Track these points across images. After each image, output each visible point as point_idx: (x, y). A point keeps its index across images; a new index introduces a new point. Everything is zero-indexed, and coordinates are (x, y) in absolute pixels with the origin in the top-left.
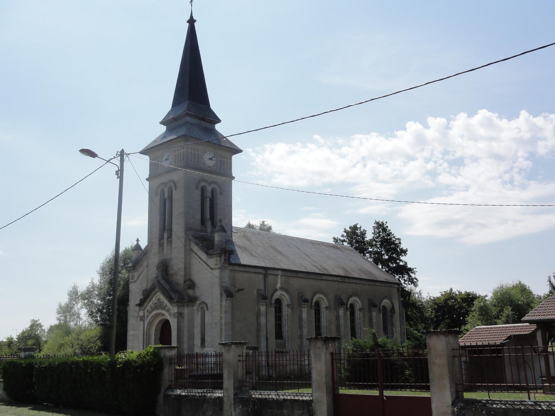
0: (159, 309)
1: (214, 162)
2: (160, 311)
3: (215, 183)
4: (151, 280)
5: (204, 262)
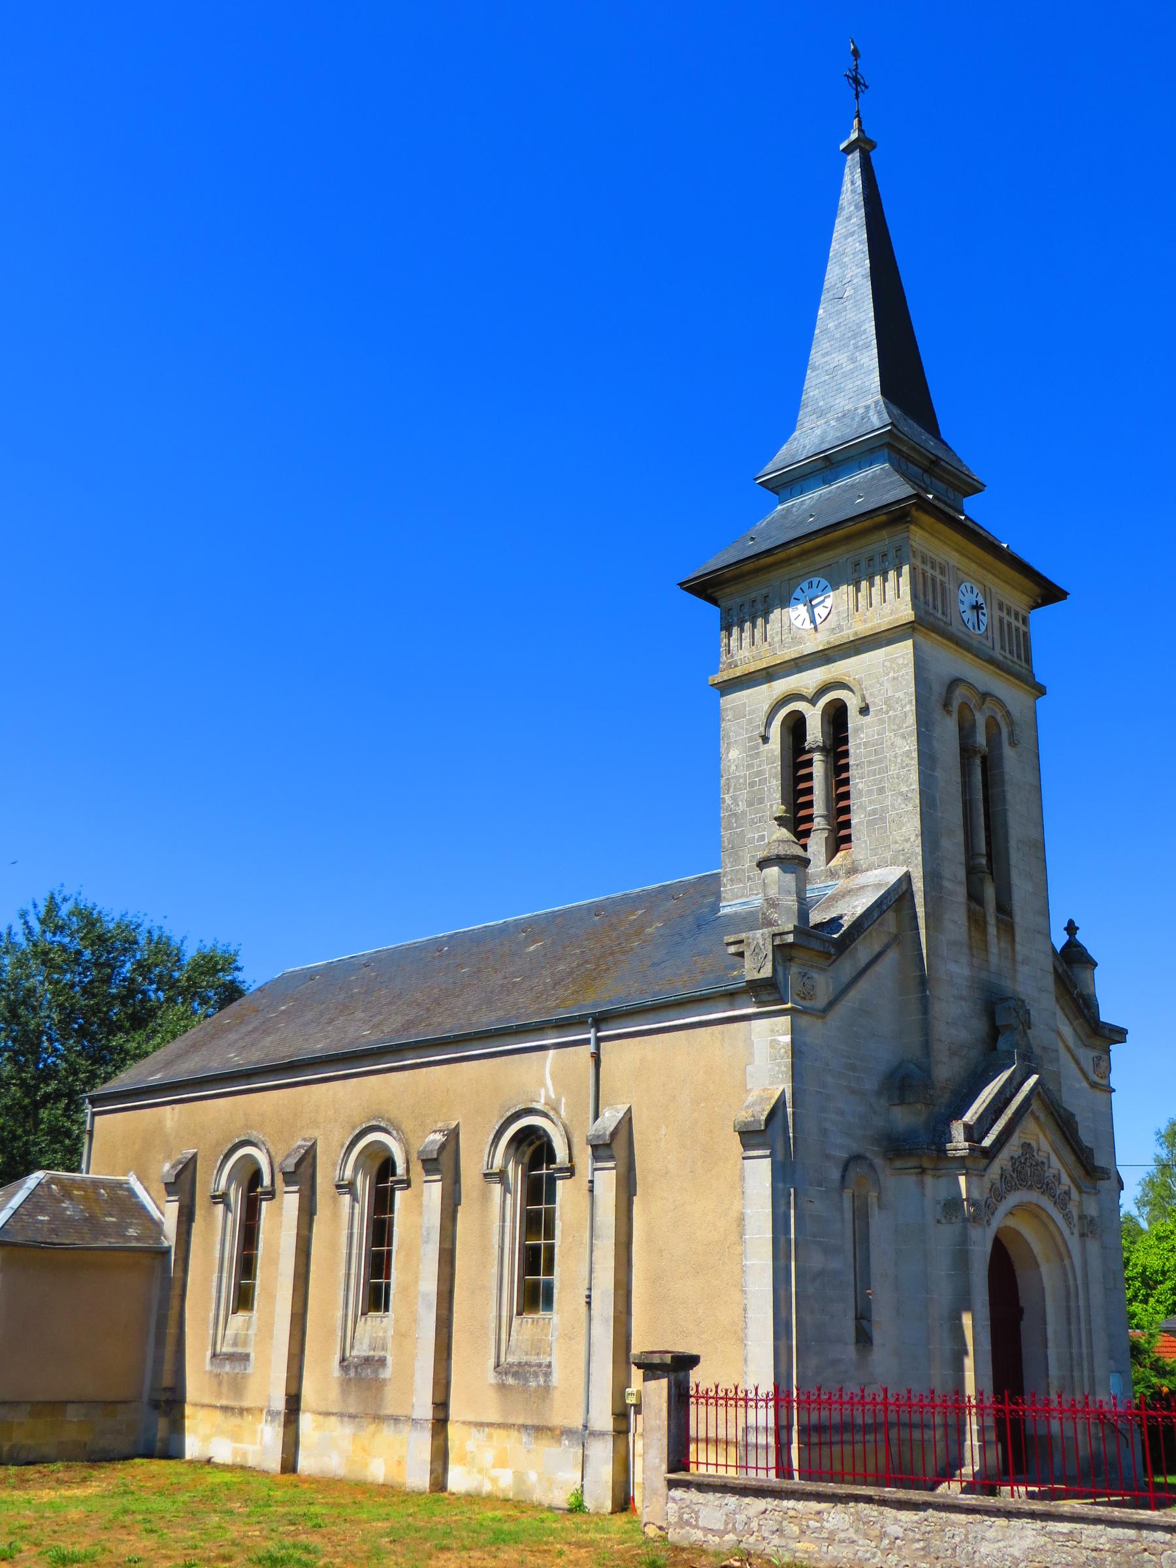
0: (1030, 1187)
2: (1033, 1196)
3: (999, 701)
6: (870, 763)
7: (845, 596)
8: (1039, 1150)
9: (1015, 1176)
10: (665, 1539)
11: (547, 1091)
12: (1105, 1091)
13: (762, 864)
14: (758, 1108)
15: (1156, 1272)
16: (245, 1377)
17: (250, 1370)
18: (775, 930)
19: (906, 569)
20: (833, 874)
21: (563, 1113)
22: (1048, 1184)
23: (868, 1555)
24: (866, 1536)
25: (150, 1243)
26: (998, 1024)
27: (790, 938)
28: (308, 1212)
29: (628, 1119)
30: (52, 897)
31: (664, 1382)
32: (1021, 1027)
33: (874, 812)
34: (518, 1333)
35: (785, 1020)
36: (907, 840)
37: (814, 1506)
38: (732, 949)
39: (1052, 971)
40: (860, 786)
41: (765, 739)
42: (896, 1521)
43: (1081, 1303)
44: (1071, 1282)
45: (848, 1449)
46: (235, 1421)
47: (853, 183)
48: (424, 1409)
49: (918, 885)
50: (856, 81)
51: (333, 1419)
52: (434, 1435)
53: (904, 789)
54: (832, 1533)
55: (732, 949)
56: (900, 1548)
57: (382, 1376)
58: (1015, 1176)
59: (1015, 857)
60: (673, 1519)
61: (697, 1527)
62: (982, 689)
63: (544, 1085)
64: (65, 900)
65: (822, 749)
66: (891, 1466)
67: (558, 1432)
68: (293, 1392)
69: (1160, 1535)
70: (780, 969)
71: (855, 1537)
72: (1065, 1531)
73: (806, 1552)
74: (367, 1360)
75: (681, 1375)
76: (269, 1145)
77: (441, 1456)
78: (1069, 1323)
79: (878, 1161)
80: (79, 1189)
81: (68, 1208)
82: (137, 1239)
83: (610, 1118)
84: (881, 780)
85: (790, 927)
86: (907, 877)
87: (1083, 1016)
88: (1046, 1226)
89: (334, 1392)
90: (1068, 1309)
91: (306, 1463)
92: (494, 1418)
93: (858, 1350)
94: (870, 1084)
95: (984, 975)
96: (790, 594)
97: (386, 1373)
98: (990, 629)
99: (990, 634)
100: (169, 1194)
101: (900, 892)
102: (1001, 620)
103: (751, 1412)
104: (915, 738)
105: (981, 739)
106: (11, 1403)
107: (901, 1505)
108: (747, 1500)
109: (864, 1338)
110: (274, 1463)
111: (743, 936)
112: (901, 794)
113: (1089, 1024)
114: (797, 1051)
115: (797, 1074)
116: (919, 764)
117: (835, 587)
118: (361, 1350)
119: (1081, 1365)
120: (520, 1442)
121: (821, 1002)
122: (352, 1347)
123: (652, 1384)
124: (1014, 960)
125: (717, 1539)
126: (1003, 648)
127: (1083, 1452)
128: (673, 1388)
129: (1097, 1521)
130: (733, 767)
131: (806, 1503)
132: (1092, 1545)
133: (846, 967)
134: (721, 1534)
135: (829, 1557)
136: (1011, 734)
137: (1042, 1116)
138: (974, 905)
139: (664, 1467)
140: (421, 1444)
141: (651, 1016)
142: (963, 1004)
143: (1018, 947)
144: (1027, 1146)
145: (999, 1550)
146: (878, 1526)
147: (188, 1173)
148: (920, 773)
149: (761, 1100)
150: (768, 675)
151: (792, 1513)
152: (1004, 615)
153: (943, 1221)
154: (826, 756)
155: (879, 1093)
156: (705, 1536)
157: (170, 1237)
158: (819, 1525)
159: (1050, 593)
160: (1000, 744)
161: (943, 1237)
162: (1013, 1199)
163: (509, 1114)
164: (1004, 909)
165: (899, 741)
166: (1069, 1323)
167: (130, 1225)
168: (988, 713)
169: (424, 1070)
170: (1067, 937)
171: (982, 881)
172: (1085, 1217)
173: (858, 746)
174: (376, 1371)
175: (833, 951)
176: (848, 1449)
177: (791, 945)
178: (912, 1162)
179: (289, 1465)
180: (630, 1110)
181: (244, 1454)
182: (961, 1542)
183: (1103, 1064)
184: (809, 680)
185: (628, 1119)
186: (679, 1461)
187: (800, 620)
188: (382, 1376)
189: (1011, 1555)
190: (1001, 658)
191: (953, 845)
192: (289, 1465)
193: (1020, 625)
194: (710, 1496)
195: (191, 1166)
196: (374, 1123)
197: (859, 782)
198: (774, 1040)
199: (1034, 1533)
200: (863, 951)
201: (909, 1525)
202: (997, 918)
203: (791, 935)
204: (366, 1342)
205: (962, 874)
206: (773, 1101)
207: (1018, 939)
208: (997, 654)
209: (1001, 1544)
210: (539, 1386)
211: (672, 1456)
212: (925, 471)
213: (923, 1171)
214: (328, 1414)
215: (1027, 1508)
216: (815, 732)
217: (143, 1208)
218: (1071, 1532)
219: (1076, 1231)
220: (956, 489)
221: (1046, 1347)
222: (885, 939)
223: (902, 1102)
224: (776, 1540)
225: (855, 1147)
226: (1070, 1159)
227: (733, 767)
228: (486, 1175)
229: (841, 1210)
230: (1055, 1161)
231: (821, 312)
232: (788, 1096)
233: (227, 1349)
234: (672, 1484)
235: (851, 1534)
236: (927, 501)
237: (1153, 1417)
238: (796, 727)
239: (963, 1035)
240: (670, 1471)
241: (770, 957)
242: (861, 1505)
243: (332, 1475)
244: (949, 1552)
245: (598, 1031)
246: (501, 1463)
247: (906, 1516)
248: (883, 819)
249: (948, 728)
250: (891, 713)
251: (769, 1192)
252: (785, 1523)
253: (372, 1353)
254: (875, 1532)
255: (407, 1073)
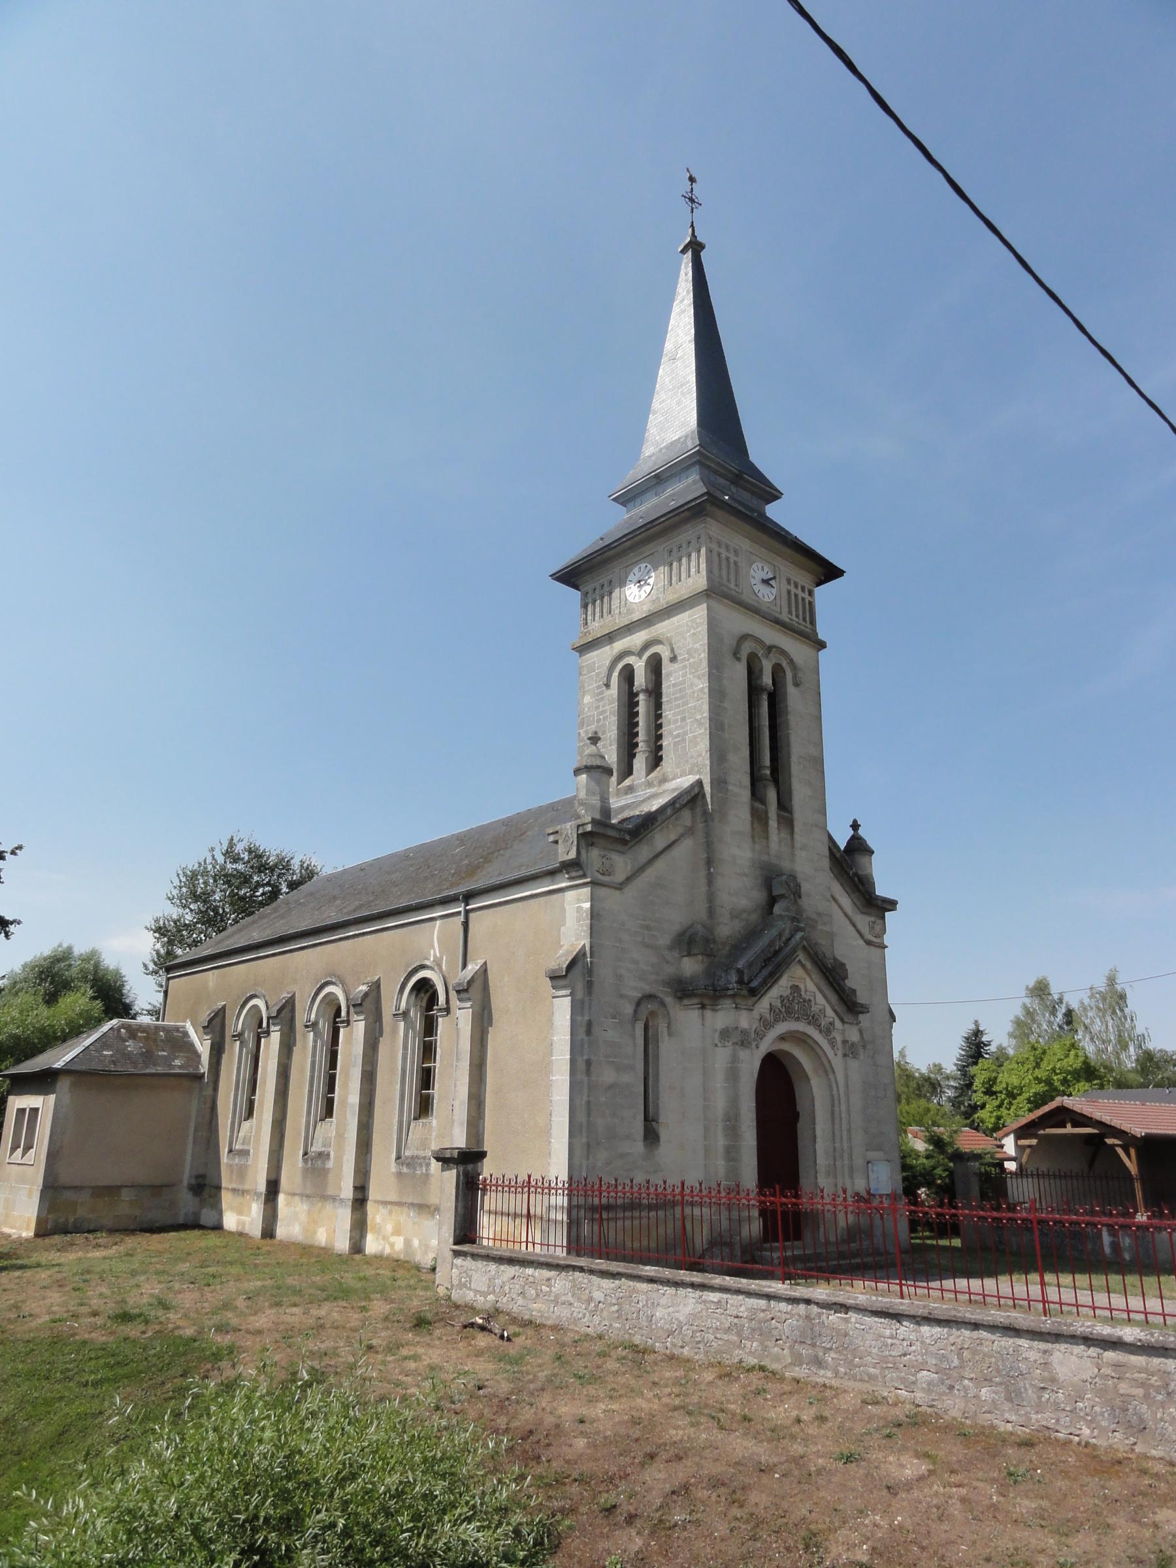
0: (798, 1019)
1: (774, 591)
2: (800, 1026)
3: (783, 652)
4: (731, 914)
5: (846, 915)
6: (676, 699)
7: (662, 576)
8: (806, 991)
9: (783, 1010)
10: (450, 1297)
11: (435, 952)
12: (879, 947)
13: (577, 772)
14: (563, 959)
15: (1016, 1087)
16: (246, 1167)
17: (249, 1162)
18: (579, 822)
19: (703, 551)
20: (649, 785)
21: (444, 967)
22: (813, 1017)
23: (580, 1315)
24: (579, 1300)
25: (191, 1070)
26: (774, 894)
27: (589, 828)
28: (287, 1047)
29: (484, 970)
30: (232, 839)
31: (454, 1171)
32: (792, 896)
33: (678, 736)
34: (413, 1133)
35: (587, 891)
36: (700, 755)
37: (546, 1273)
38: (551, 838)
39: (827, 853)
40: (669, 717)
41: (607, 686)
42: (600, 1288)
43: (843, 1108)
44: (835, 1092)
45: (628, 1223)
46: (239, 1199)
47: (686, 275)
48: (347, 1192)
49: (707, 788)
50: (692, 200)
51: (297, 1198)
52: (354, 1209)
53: (698, 717)
54: (557, 1296)
55: (551, 838)
56: (602, 1310)
57: (327, 1167)
58: (783, 1010)
59: (795, 769)
60: (455, 1282)
61: (470, 1289)
62: (768, 642)
63: (433, 947)
64: (241, 840)
65: (646, 691)
66: (603, 1241)
67: (432, 1209)
68: (273, 1177)
69: (783, 1306)
70: (583, 852)
71: (572, 1300)
72: (715, 1300)
73: (540, 1311)
74: (320, 1154)
75: (470, 1167)
76: (267, 998)
77: (360, 1226)
78: (833, 1124)
79: (669, 1000)
80: (142, 1032)
81: (131, 1046)
82: (180, 1067)
83: (473, 968)
84: (683, 712)
85: (589, 819)
86: (699, 783)
87: (859, 890)
88: (813, 1049)
89: (298, 1178)
90: (833, 1113)
91: (281, 1232)
92: (393, 1197)
93: (646, 1146)
94: (664, 940)
95: (765, 858)
96: (627, 578)
97: (330, 1164)
98: (778, 599)
99: (778, 601)
100: (206, 1034)
101: (693, 794)
102: (789, 592)
103: (553, 1198)
104: (707, 678)
105: (767, 680)
106: (76, 1187)
107: (604, 1274)
108: (502, 1267)
109: (651, 1135)
110: (256, 1231)
111: (558, 828)
112: (697, 720)
113: (865, 898)
114: (594, 914)
115: (593, 932)
116: (710, 697)
117: (655, 568)
118: (316, 1148)
119: (842, 1157)
120: (409, 1216)
121: (619, 877)
122: (312, 1145)
123: (447, 1173)
124: (793, 846)
125: (482, 1298)
126: (790, 612)
127: (842, 1223)
128: (461, 1178)
129: (738, 1292)
130: (586, 709)
131: (541, 1271)
132: (735, 1313)
133: (644, 852)
134: (484, 1294)
135: (554, 1316)
136: (795, 677)
137: (809, 965)
138: (758, 805)
139: (451, 1240)
140: (344, 1216)
141: (502, 892)
142: (745, 879)
143: (797, 837)
144: (795, 988)
145: (669, 1314)
146: (587, 1291)
147: (218, 1020)
148: (710, 703)
149: (568, 952)
150: (610, 638)
151: (531, 1279)
152: (792, 588)
153: (719, 1045)
154: (650, 696)
155: (671, 948)
156: (475, 1296)
157: (204, 1067)
158: (548, 1289)
159: (830, 572)
160: (784, 685)
161: (721, 1056)
162: (782, 1028)
163: (410, 969)
164: (784, 805)
165: (696, 681)
166: (833, 1124)
167: (176, 1058)
168: (774, 661)
169: (361, 938)
170: (852, 832)
171: (765, 786)
172: (847, 1041)
173: (669, 687)
174: (324, 1163)
175: (628, 838)
176: (628, 1223)
177: (590, 833)
178: (695, 1001)
179: (268, 1233)
180: (485, 963)
181: (244, 1224)
182: (643, 1306)
183: (878, 928)
184: (638, 639)
185: (484, 970)
186: (465, 1235)
187: (633, 595)
188: (327, 1167)
189: (677, 1319)
190: (787, 620)
191: (739, 759)
192: (268, 1233)
193: (806, 595)
194: (480, 1264)
195: (221, 1014)
196: (329, 979)
197: (669, 713)
198: (580, 907)
199: (694, 1301)
200: (659, 840)
201: (608, 1292)
202: (779, 816)
203: (590, 825)
204: (320, 1141)
205: (746, 781)
206: (575, 953)
207: (796, 830)
208: (785, 617)
209: (671, 1309)
210: (422, 1174)
211: (458, 1231)
212: (732, 483)
213: (703, 1007)
214: (294, 1194)
215: (688, 1279)
216: (641, 679)
217: (192, 1045)
218: (719, 1302)
219: (840, 1053)
220: (760, 497)
221: (815, 1142)
222: (680, 830)
223: (689, 955)
224: (520, 1301)
225: (649, 989)
226: (834, 998)
227: (586, 709)
228: (394, 1015)
229: (633, 1037)
230: (820, 999)
231: (661, 371)
232: (588, 949)
233: (238, 1147)
234: (457, 1254)
235: (569, 1298)
236: (724, 502)
237: (785, 1204)
238: (628, 675)
239: (744, 903)
240: (455, 1244)
241: (575, 843)
242: (577, 1274)
243: (294, 1240)
244: (635, 1315)
245: (467, 904)
246: (397, 1232)
247: (607, 1284)
248: (684, 740)
249: (739, 671)
250: (691, 660)
251: (568, 1023)
252: (526, 1287)
253: (323, 1149)
254: (585, 1297)
255: (350, 941)
